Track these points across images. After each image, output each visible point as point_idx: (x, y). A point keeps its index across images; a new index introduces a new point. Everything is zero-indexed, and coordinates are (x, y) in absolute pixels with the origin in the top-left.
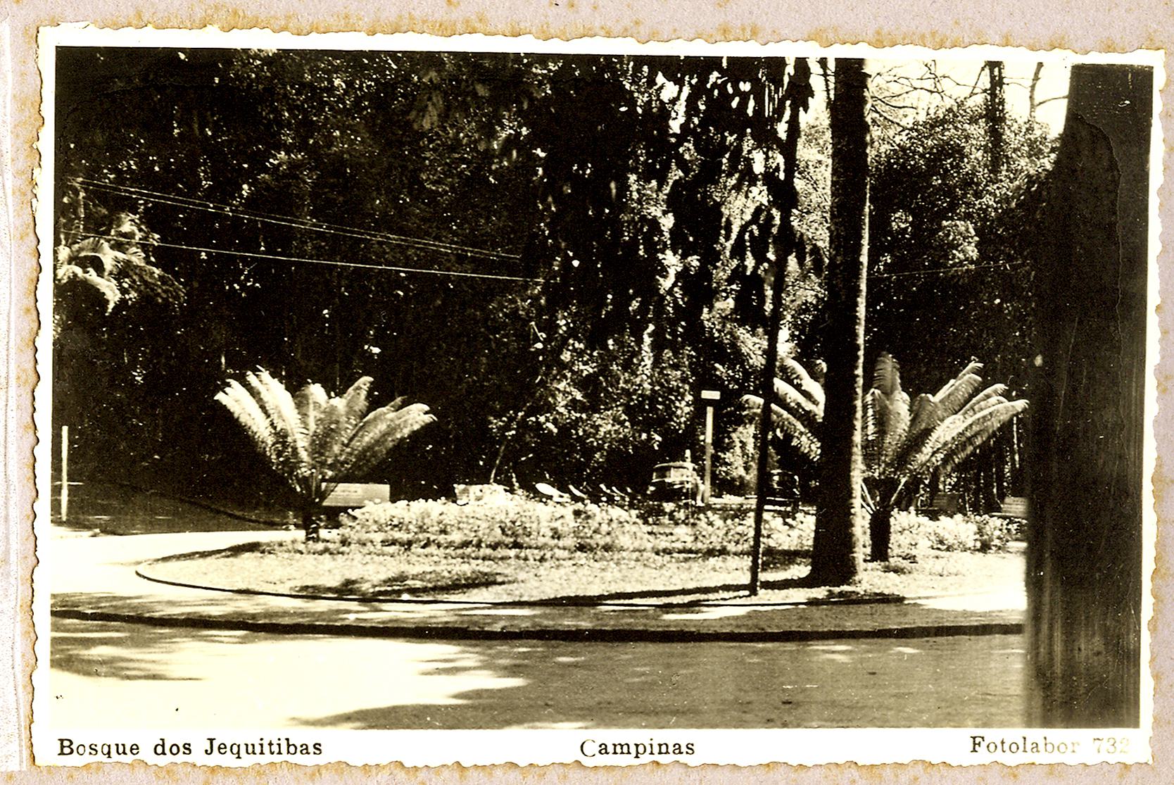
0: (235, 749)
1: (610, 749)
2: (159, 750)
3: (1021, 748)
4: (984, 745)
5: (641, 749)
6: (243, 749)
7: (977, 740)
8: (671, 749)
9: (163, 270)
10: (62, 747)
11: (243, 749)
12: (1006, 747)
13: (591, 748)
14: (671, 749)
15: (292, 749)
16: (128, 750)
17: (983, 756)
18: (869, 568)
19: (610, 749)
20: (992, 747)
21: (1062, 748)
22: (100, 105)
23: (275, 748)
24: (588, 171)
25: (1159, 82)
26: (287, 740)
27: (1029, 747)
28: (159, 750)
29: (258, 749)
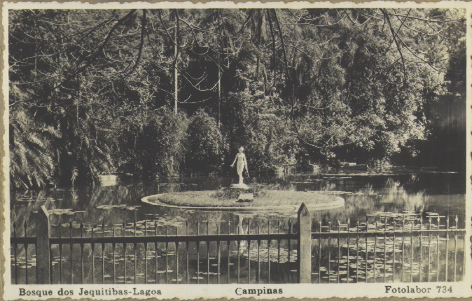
0: (39, 293)
1: (248, 292)
2: (60, 293)
3: (407, 291)
4: (391, 289)
5: (260, 292)
6: (95, 293)
7: (388, 288)
8: (273, 291)
9: (428, 193)
10: (21, 292)
11: (95, 293)
12: (400, 290)
13: (240, 292)
14: (273, 291)
15: (115, 293)
16: (48, 293)
17: (390, 294)
18: (335, 194)
19: (248, 292)
20: (394, 291)
21: (424, 291)
22: (129, 260)
23: (108, 292)
24: (119, 149)
25: (7, 275)
26: (439, 292)
27: (410, 290)
28: (60, 293)
29: (101, 293)
